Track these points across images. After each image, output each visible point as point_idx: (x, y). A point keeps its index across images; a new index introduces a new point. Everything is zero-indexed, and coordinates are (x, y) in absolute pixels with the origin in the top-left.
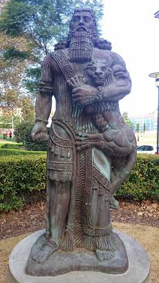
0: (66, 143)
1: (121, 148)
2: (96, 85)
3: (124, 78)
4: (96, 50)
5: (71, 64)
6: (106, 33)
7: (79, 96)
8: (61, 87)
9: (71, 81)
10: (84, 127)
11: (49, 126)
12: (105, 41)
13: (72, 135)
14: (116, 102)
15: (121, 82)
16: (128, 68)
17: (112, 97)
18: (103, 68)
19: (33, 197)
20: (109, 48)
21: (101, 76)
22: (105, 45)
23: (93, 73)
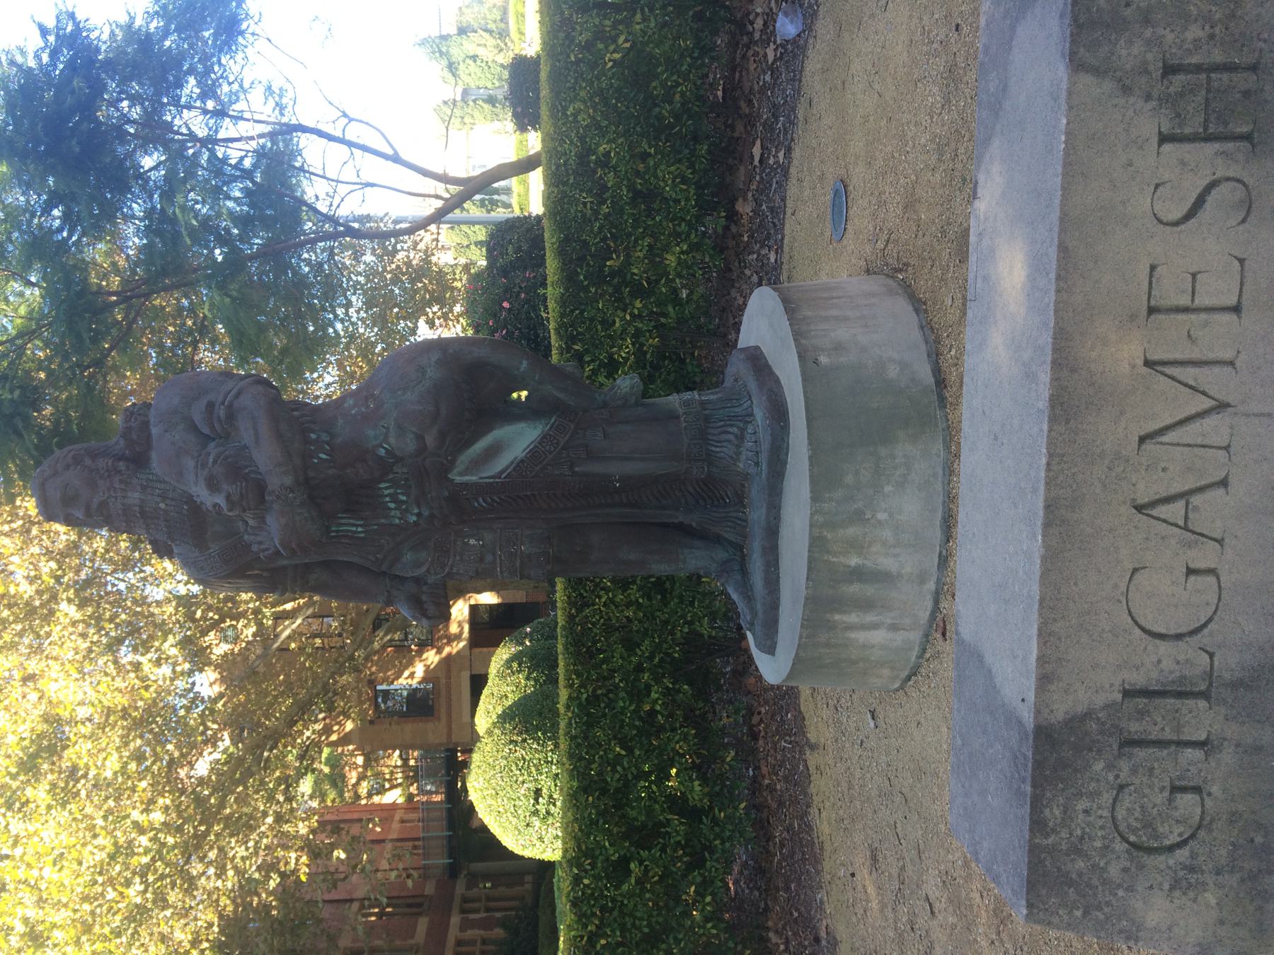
10: (392, 505)
18: (213, 485)
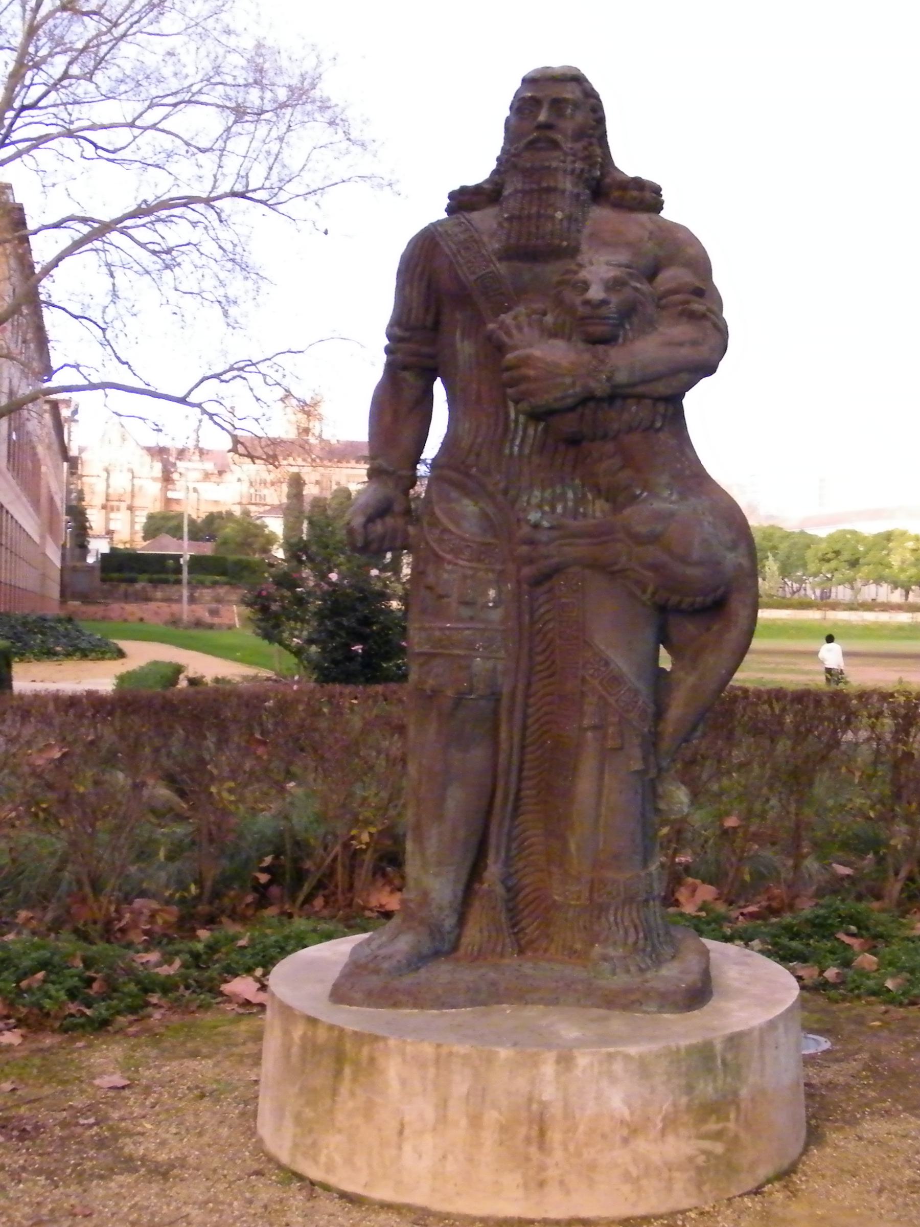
0: (482, 553)
1: (691, 571)
2: (594, 341)
3: (693, 317)
4: (600, 214)
5: (502, 268)
6: (629, 155)
7: (526, 379)
8: (465, 349)
9: (502, 325)
11: (420, 489)
12: (639, 183)
13: (501, 525)
14: (674, 402)
15: (682, 330)
16: (720, 279)
17: (644, 382)
18: (614, 285)
19: (773, 844)
20: (656, 205)
21: (603, 311)
22: (645, 197)
23: (578, 300)
